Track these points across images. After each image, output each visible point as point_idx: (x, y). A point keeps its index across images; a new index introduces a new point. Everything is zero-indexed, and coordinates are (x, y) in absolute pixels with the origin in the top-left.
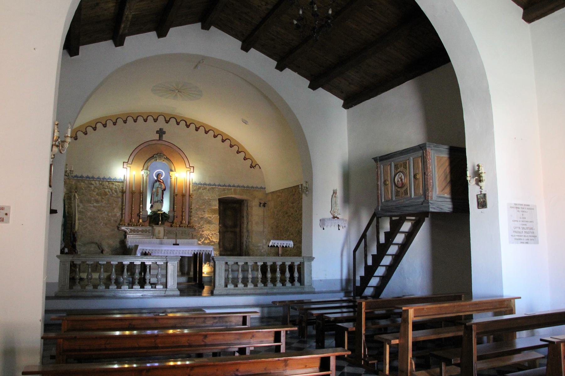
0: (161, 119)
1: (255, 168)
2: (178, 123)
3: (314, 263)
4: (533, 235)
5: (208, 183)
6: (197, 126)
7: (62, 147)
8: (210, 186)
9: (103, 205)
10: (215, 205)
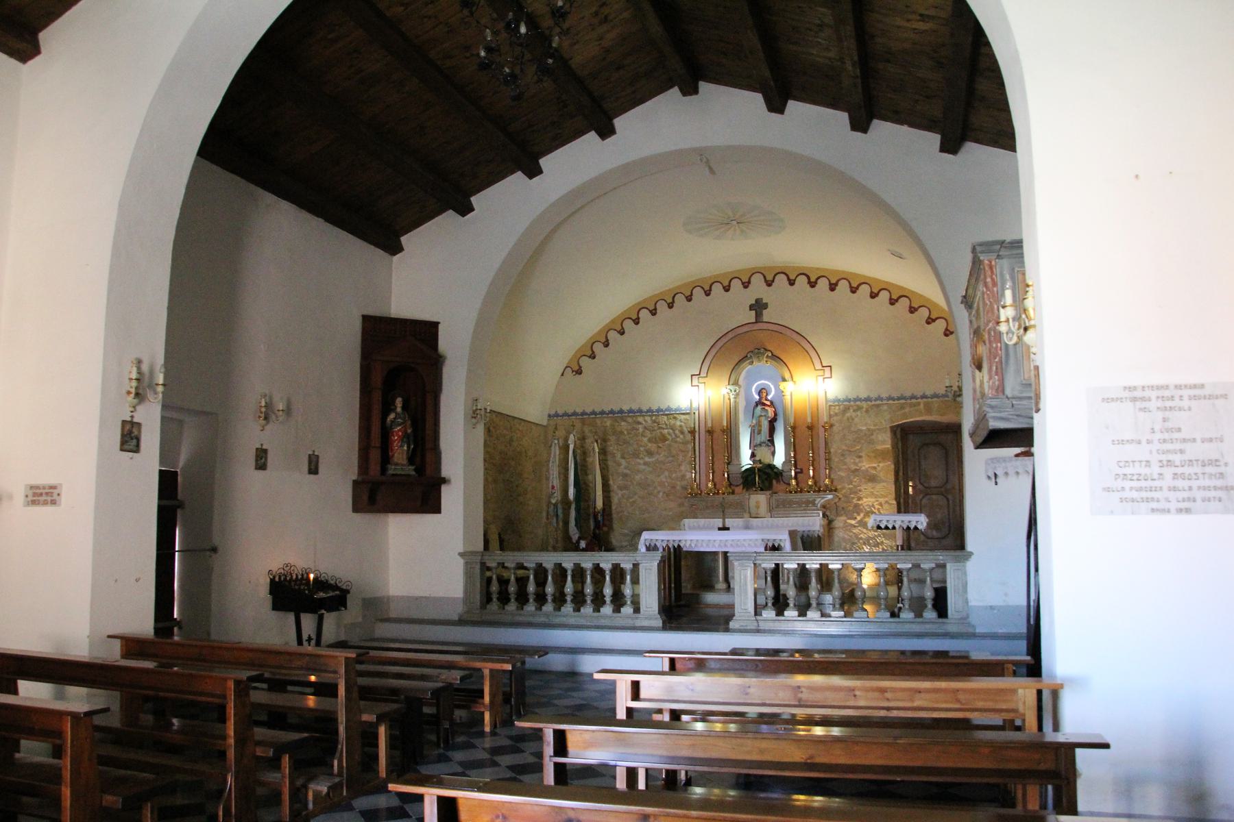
0: (757, 280)
2: (792, 283)
3: (970, 565)
4: (1219, 483)
5: (863, 395)
6: (833, 281)
7: (510, 446)
8: (869, 403)
10: (883, 442)
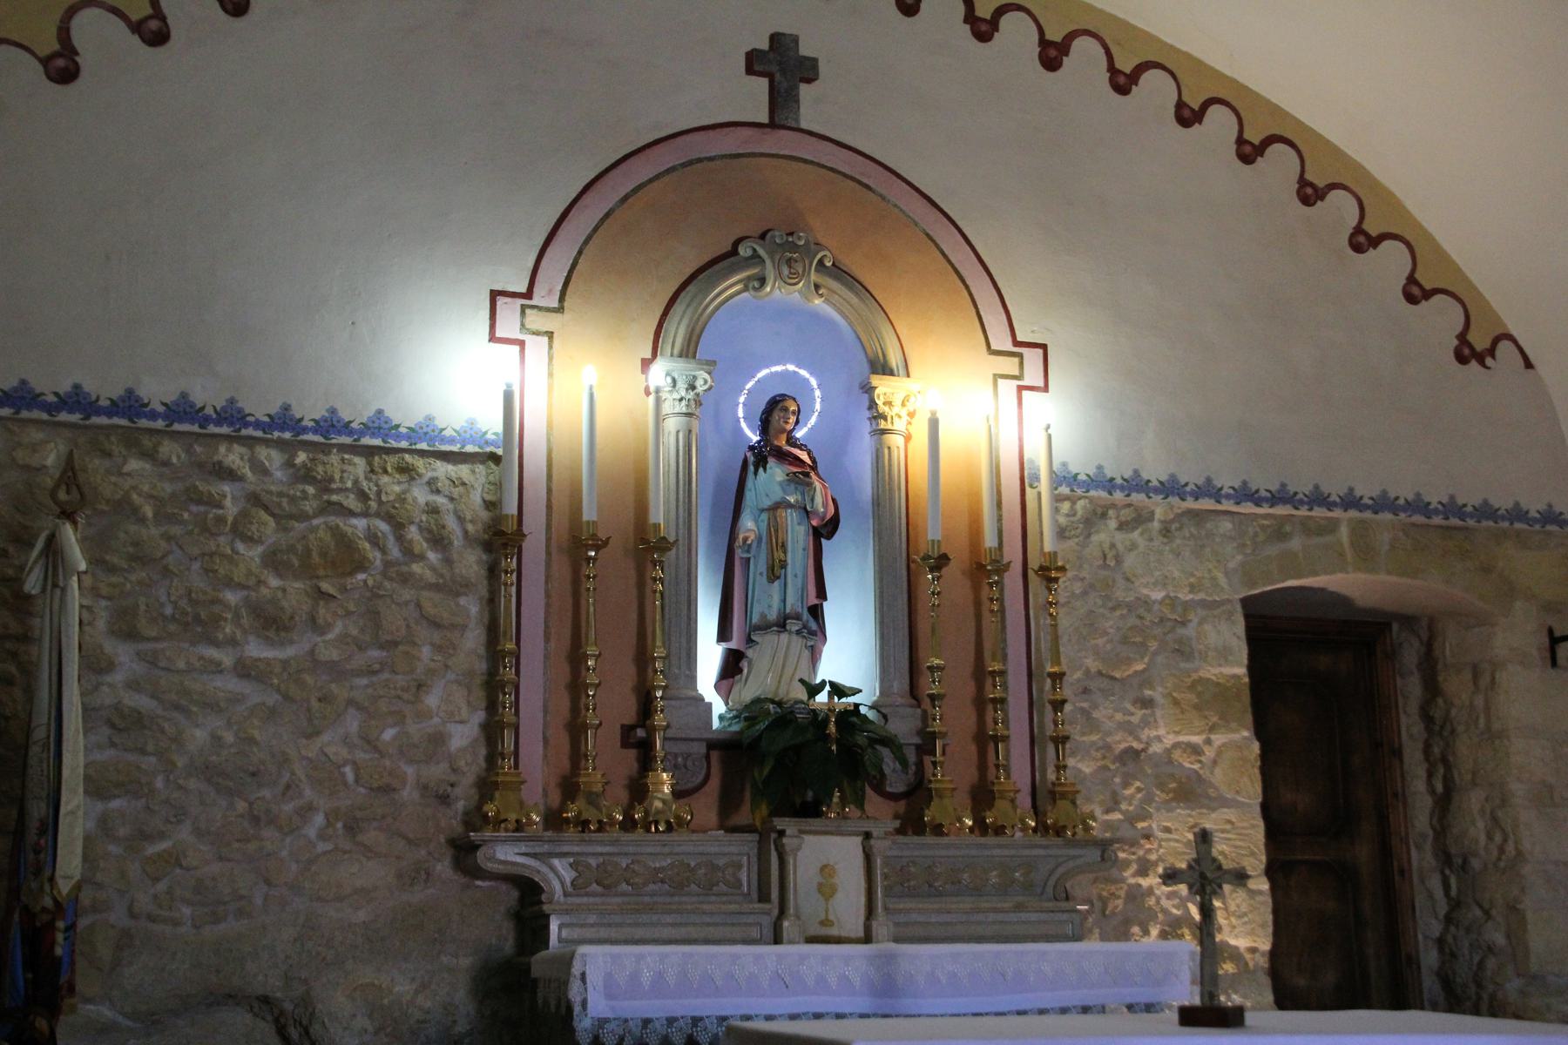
1: (1489, 361)
5: (1155, 473)
6: (1055, 35)
9: (330, 654)
10: (1224, 655)
